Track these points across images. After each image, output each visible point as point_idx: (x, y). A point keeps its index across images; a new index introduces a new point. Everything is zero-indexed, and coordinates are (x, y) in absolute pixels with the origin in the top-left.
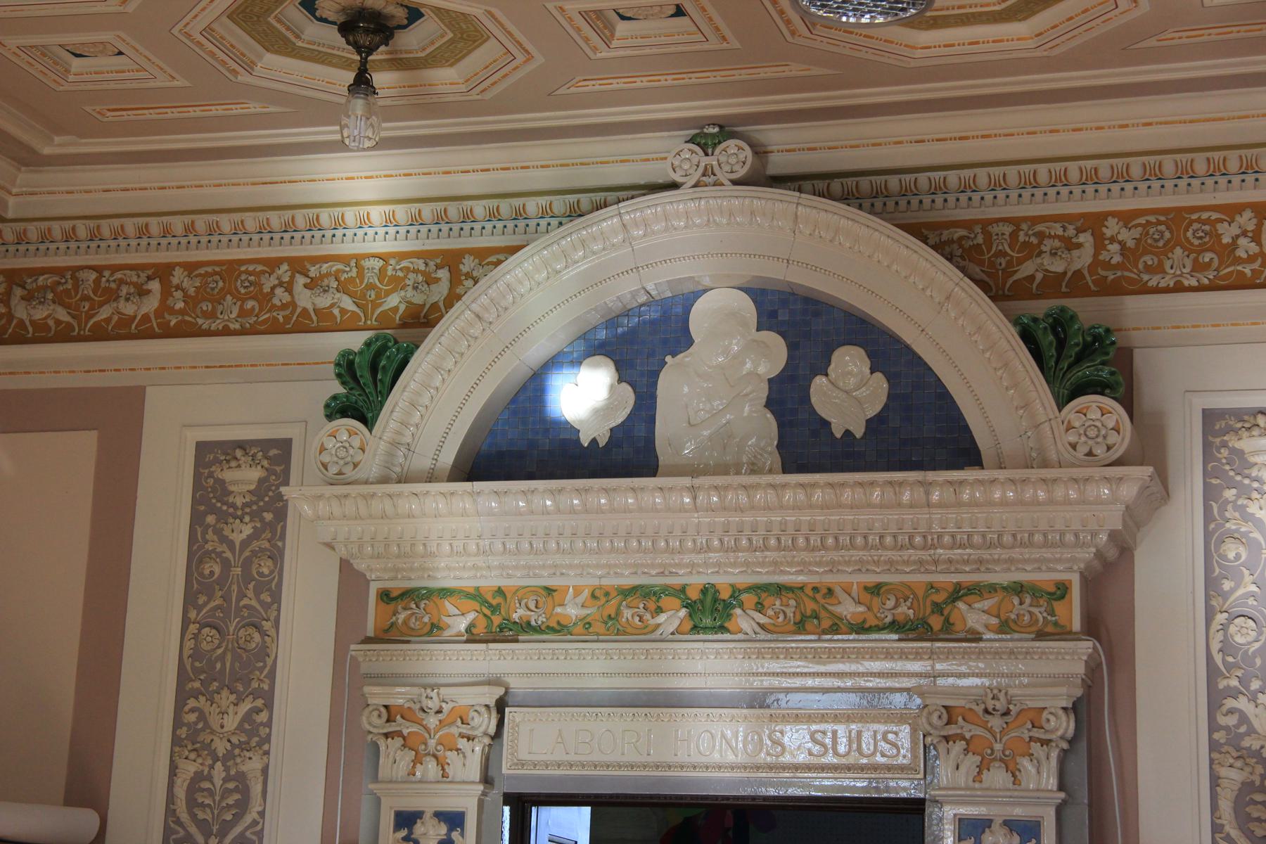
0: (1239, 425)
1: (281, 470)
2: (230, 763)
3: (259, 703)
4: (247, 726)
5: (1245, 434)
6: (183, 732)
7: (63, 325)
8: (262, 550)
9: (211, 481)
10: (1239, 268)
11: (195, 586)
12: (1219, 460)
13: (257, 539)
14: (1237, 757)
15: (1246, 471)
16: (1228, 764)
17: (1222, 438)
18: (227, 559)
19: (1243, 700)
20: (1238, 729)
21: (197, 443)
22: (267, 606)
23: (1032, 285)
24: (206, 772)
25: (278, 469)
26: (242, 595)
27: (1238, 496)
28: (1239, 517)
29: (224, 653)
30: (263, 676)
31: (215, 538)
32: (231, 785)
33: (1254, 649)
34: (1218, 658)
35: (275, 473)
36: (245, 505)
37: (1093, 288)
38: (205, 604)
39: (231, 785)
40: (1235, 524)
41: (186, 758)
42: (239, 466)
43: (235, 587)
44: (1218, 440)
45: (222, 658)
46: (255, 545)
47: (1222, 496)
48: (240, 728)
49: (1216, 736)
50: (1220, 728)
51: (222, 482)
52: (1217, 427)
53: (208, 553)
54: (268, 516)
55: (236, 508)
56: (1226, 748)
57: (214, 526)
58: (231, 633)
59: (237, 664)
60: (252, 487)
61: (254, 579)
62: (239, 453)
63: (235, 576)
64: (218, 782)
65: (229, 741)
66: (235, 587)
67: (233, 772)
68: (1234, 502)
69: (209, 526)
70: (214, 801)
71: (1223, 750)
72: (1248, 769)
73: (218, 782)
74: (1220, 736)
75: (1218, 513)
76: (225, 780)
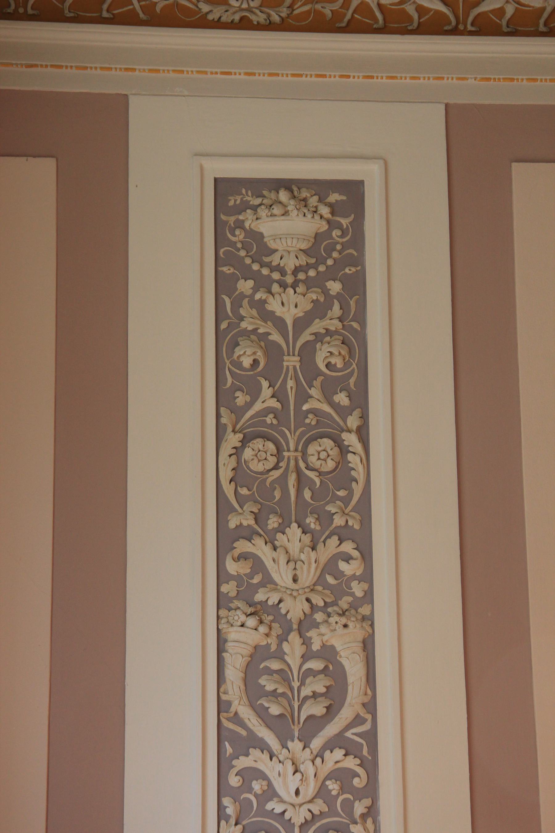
0: (258, 201)
1: (350, 223)
2: (312, 633)
3: (348, 547)
4: (330, 580)
5: (263, 212)
6: (229, 588)
7: (432, 13)
8: (328, 332)
9: (240, 235)
10: (318, 7)
11: (230, 380)
12: (233, 244)
13: (322, 317)
14: (251, 614)
15: (267, 259)
16: (239, 623)
17: (236, 216)
18: (274, 343)
19: (259, 542)
20: (253, 578)
21: (362, 182)
22: (343, 412)
23: (63, 5)
24: (274, 647)
25: (344, 222)
26: (306, 397)
27: (255, 289)
28: (256, 315)
29: (285, 476)
30: (350, 508)
31: (254, 312)
32: (316, 665)
33: (272, 478)
34: (229, 490)
35: (339, 226)
36: (296, 271)
37: (142, 15)
38: (249, 405)
39: (316, 665)
40: (251, 323)
41: (242, 626)
42: (286, 213)
43: (291, 383)
44: (232, 219)
45: (283, 480)
46: (318, 326)
47: (236, 289)
48: (320, 580)
49: (224, 588)
50: (230, 578)
51: (258, 237)
52: (231, 203)
53: (246, 333)
54: (335, 287)
55: (283, 273)
56: (237, 603)
57: (252, 296)
58: (292, 446)
59: (307, 494)
60: (304, 246)
61: (322, 374)
62: (283, 196)
63: (291, 368)
64: (294, 660)
65: (308, 600)
66: (291, 383)
67: (316, 647)
68: (252, 296)
69: (242, 296)
70: (291, 689)
71: (232, 605)
72: (263, 629)
73: (294, 660)
74: (229, 588)
75: (231, 309)
76: (305, 658)
